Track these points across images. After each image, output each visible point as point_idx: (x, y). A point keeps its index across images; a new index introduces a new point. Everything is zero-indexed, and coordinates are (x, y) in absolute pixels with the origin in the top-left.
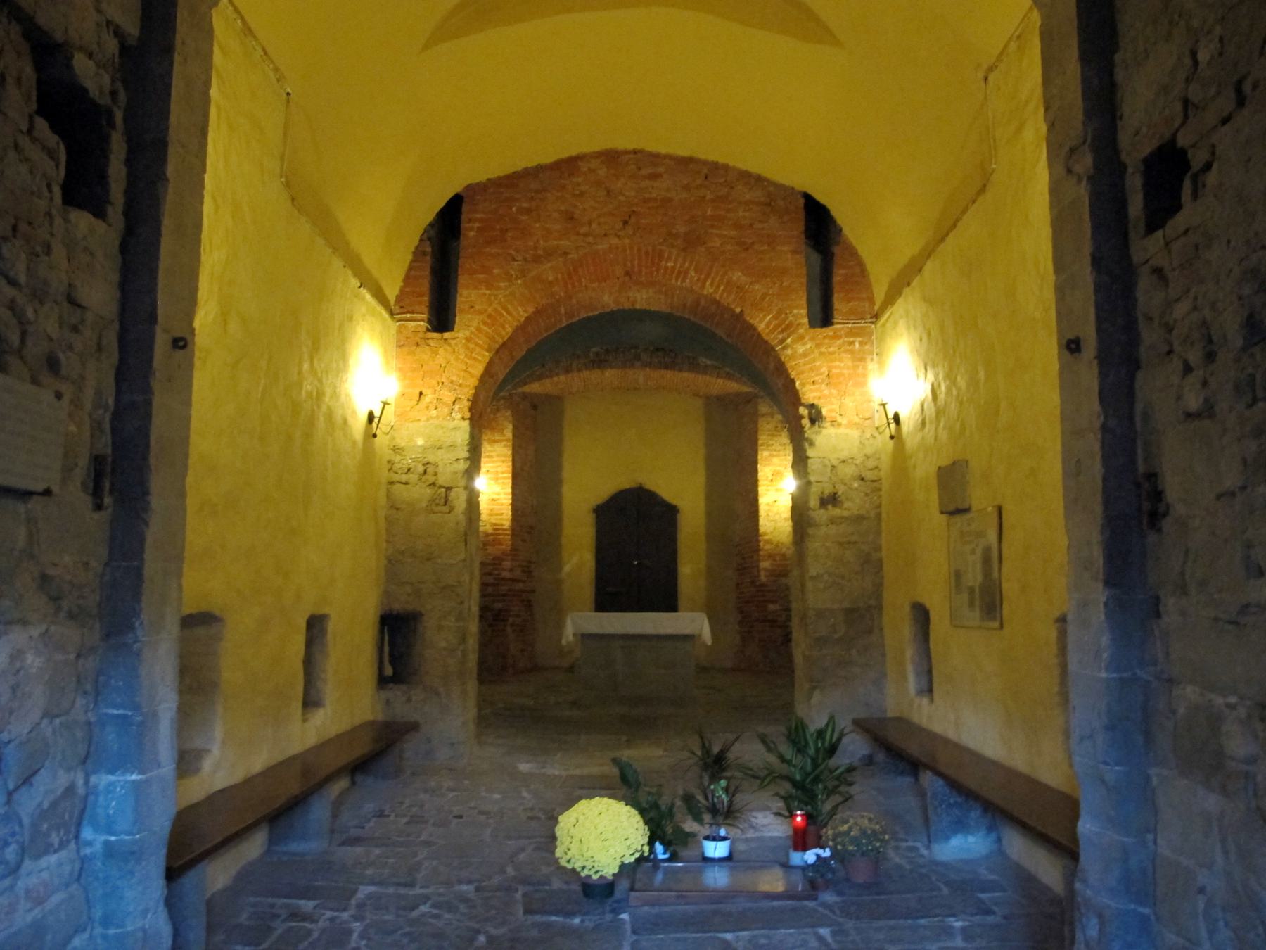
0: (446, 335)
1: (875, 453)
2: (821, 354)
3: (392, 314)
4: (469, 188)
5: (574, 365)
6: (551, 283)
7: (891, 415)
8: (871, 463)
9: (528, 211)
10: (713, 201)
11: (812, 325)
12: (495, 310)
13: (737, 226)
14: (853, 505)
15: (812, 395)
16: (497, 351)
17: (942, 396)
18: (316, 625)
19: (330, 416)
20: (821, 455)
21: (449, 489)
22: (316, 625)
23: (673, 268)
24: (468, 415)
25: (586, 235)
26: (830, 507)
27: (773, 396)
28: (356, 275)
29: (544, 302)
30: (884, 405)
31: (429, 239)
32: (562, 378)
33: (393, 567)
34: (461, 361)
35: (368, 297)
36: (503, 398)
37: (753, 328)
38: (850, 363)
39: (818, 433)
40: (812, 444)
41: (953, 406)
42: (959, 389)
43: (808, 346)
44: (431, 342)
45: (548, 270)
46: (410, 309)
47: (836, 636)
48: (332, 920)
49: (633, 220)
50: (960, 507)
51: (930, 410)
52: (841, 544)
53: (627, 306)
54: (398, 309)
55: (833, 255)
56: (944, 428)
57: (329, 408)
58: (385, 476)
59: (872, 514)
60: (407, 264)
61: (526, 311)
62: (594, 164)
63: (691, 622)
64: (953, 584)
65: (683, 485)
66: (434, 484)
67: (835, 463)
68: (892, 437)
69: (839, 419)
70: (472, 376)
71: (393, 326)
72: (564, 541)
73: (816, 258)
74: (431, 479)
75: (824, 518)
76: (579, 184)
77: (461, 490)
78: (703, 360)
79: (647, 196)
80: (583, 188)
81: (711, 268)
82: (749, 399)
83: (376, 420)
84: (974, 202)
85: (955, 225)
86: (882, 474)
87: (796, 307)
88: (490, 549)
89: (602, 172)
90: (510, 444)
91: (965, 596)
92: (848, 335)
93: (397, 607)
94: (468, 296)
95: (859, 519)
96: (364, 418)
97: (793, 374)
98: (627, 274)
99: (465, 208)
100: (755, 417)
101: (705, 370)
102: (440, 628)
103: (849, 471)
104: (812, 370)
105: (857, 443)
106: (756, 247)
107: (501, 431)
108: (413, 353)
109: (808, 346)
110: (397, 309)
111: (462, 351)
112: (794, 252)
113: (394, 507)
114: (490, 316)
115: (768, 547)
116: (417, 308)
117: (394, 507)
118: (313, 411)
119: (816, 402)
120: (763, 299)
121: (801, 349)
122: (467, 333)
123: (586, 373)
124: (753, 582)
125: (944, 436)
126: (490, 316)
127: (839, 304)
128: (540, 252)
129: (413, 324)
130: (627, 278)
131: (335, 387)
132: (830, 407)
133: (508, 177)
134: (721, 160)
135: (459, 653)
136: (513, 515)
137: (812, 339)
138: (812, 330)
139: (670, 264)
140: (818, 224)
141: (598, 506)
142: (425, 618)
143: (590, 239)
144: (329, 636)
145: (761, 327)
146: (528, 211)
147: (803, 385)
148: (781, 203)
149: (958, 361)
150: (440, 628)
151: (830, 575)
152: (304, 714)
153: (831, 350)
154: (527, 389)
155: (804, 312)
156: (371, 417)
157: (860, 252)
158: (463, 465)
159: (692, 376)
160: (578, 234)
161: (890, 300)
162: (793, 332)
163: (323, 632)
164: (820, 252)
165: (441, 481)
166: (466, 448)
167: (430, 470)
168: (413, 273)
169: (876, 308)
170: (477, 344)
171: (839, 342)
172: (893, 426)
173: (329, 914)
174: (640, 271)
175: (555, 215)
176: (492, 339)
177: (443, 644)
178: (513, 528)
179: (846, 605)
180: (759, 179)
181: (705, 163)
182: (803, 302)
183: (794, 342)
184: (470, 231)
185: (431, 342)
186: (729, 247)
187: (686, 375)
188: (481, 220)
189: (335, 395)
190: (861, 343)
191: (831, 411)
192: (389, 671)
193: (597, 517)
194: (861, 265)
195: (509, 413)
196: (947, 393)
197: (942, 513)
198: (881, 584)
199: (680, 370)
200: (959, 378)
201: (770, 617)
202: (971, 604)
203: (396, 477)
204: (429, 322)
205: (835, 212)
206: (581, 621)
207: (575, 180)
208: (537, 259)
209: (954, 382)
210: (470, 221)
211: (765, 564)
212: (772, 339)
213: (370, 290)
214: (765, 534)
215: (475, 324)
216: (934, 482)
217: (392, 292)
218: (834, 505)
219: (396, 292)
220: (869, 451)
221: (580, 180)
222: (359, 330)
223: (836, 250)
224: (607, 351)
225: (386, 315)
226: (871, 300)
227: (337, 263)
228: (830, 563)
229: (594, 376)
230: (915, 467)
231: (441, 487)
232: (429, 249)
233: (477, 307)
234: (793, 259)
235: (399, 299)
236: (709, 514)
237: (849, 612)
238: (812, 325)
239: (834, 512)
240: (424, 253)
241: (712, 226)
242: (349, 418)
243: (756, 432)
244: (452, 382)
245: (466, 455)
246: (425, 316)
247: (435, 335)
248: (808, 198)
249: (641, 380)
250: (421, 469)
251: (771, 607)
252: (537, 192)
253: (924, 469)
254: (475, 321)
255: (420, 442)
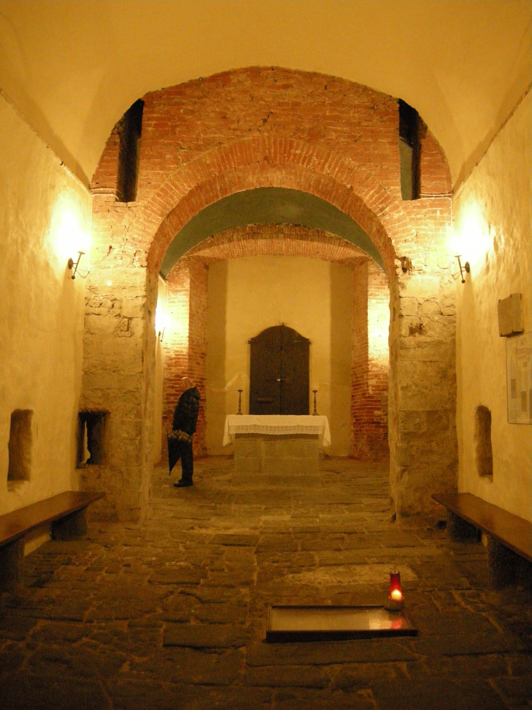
0: (130, 204)
1: (451, 295)
2: (412, 219)
3: (89, 188)
4: (149, 95)
5: (235, 237)
6: (208, 165)
7: (463, 265)
8: (448, 302)
9: (193, 112)
10: (331, 105)
11: (405, 198)
12: (167, 185)
13: (349, 123)
14: (434, 333)
15: (404, 250)
16: (168, 216)
17: (502, 246)
18: (20, 420)
19: (33, 259)
20: (410, 295)
21: (130, 319)
22: (20, 420)
23: (300, 155)
24: (145, 264)
25: (234, 130)
26: (417, 334)
27: (377, 257)
28: (57, 154)
29: (204, 179)
30: (458, 257)
31: (119, 133)
32: (226, 245)
33: (88, 375)
34: (141, 223)
35: (69, 173)
36: (184, 260)
37: (358, 199)
38: (433, 227)
39: (408, 279)
40: (403, 287)
41: (511, 254)
42: (515, 240)
43: (402, 213)
44: (119, 210)
45: (207, 156)
46: (103, 184)
47: (420, 432)
48: (10, 647)
49: (270, 119)
50: (515, 330)
51: (493, 257)
52: (424, 362)
53: (266, 185)
54: (94, 185)
55: (421, 146)
56: (504, 270)
57: (32, 252)
58: (83, 308)
59: (449, 340)
60: (101, 153)
61: (190, 186)
62: (242, 77)
63: (316, 423)
64: (510, 393)
65: (315, 325)
66: (119, 315)
67: (421, 301)
68: (463, 282)
69: (424, 268)
70: (149, 234)
71: (91, 197)
72: (227, 364)
73: (408, 151)
74: (117, 311)
75: (413, 343)
76: (230, 92)
77: (140, 320)
78: (328, 234)
79: (281, 101)
80: (233, 95)
81: (329, 155)
82: (363, 262)
83: (74, 266)
84: (526, 93)
85: (512, 114)
86: (456, 310)
87: (393, 185)
88: (174, 370)
89: (248, 83)
90: (188, 293)
91: (519, 400)
92: (431, 206)
93: (91, 407)
94: (145, 174)
95: (439, 343)
96: (66, 264)
97: (390, 235)
98: (266, 158)
99: (145, 109)
100: (366, 275)
101: (330, 240)
102: (123, 423)
103: (431, 308)
104: (404, 231)
105: (438, 287)
106: (363, 140)
107: (182, 284)
108: (104, 217)
109: (402, 213)
110: (94, 185)
111: (141, 215)
112: (391, 143)
113: (89, 331)
114: (162, 190)
115: (375, 369)
116: (108, 184)
117: (89, 331)
118: (18, 254)
119: (407, 255)
120: (367, 178)
121: (396, 216)
122: (145, 202)
123: (243, 243)
124: (364, 394)
125: (503, 277)
126: (162, 190)
127: (425, 183)
128: (201, 143)
129: (105, 195)
130: (266, 162)
131: (38, 238)
132: (417, 259)
133: (177, 87)
134: (337, 75)
135: (137, 442)
136: (190, 344)
137: (405, 208)
138: (405, 202)
139: (298, 152)
140: (410, 124)
141: (252, 339)
142: (112, 415)
143: (238, 133)
144: (33, 428)
145: (366, 199)
146: (193, 112)
147: (397, 242)
148: (382, 107)
149: (514, 217)
150: (123, 423)
151: (417, 386)
152: (9, 486)
153: (419, 216)
154: (201, 253)
155: (399, 188)
156: (70, 264)
157: (441, 144)
158: (141, 301)
159: (320, 244)
160: (230, 129)
161: (462, 178)
162: (390, 203)
163: (27, 424)
164: (411, 146)
165: (125, 313)
166: (143, 289)
167: (117, 305)
168: (106, 158)
169: (453, 185)
170: (153, 211)
171: (424, 211)
172: (465, 273)
173: (9, 642)
174: (275, 157)
175: (212, 115)
176: (164, 207)
177: (125, 435)
178: (190, 357)
179: (428, 409)
180: (365, 89)
181: (325, 77)
182: (398, 181)
183: (391, 210)
184: (149, 127)
185: (119, 210)
186: (342, 139)
187: (315, 243)
188: (157, 119)
189: (38, 242)
190: (441, 212)
191: (419, 262)
192: (87, 455)
193: (251, 347)
194: (441, 153)
195: (187, 271)
196: (506, 244)
197: (502, 336)
198: (455, 393)
199: (312, 240)
200: (515, 231)
201: (375, 420)
202: (524, 407)
203: (92, 310)
204: (118, 194)
205: (421, 114)
206: (239, 422)
207: (227, 89)
208: (199, 148)
209: (511, 235)
210: (149, 119)
211: (372, 382)
212: (375, 208)
213: (70, 168)
214: (373, 360)
215: (152, 195)
216: (495, 312)
217: (90, 171)
218: (420, 333)
219: (93, 172)
220: (446, 293)
221: (231, 89)
222: (60, 196)
223: (423, 142)
224: (259, 227)
225: (85, 189)
226: (449, 179)
227: (41, 145)
228: (416, 377)
229: (250, 244)
230: (481, 303)
231: (124, 317)
232: (118, 141)
233: (153, 183)
234: (392, 150)
235: (95, 177)
236: (333, 345)
237: (431, 414)
238: (405, 198)
239: (419, 338)
240: (115, 143)
241: (330, 124)
242: (51, 262)
243: (367, 285)
244: (134, 239)
245: (143, 293)
246: (115, 190)
247: (122, 204)
248: (401, 102)
249: (284, 247)
250: (110, 304)
251: (376, 413)
252: (199, 98)
253: (487, 305)
254: (152, 193)
255: (109, 283)
